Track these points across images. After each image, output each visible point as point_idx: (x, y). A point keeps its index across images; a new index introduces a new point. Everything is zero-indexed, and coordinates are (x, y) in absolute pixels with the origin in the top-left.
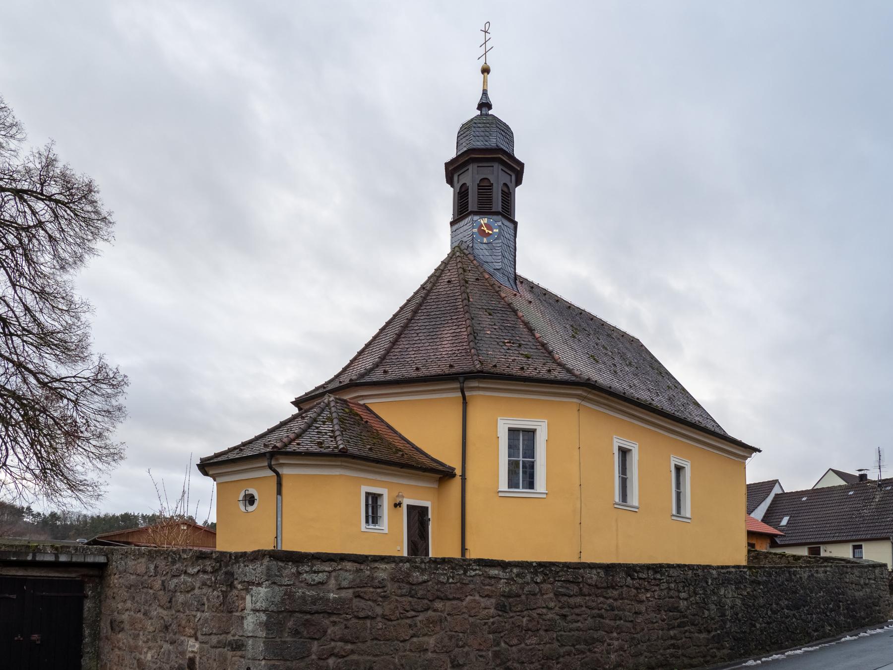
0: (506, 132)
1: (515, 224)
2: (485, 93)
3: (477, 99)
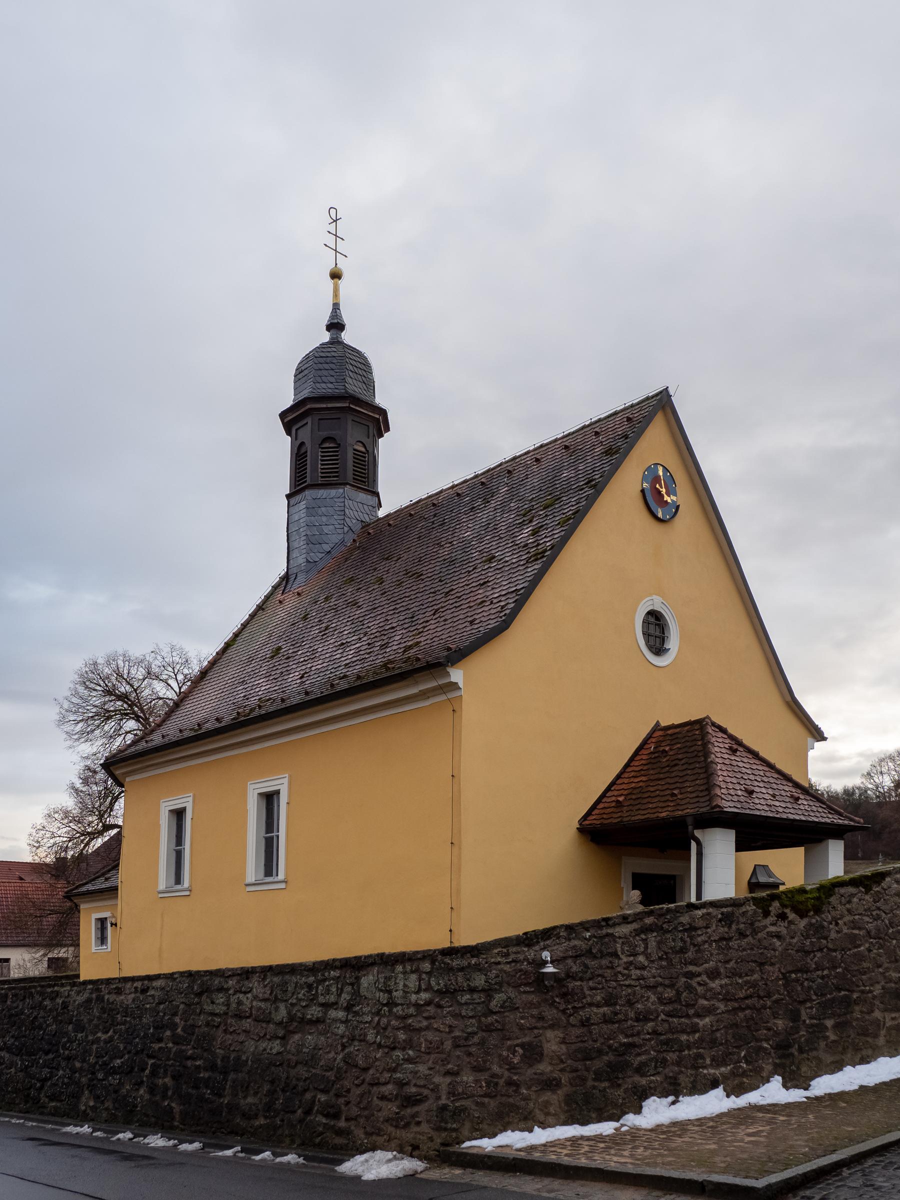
2: (336, 307)
3: (325, 319)
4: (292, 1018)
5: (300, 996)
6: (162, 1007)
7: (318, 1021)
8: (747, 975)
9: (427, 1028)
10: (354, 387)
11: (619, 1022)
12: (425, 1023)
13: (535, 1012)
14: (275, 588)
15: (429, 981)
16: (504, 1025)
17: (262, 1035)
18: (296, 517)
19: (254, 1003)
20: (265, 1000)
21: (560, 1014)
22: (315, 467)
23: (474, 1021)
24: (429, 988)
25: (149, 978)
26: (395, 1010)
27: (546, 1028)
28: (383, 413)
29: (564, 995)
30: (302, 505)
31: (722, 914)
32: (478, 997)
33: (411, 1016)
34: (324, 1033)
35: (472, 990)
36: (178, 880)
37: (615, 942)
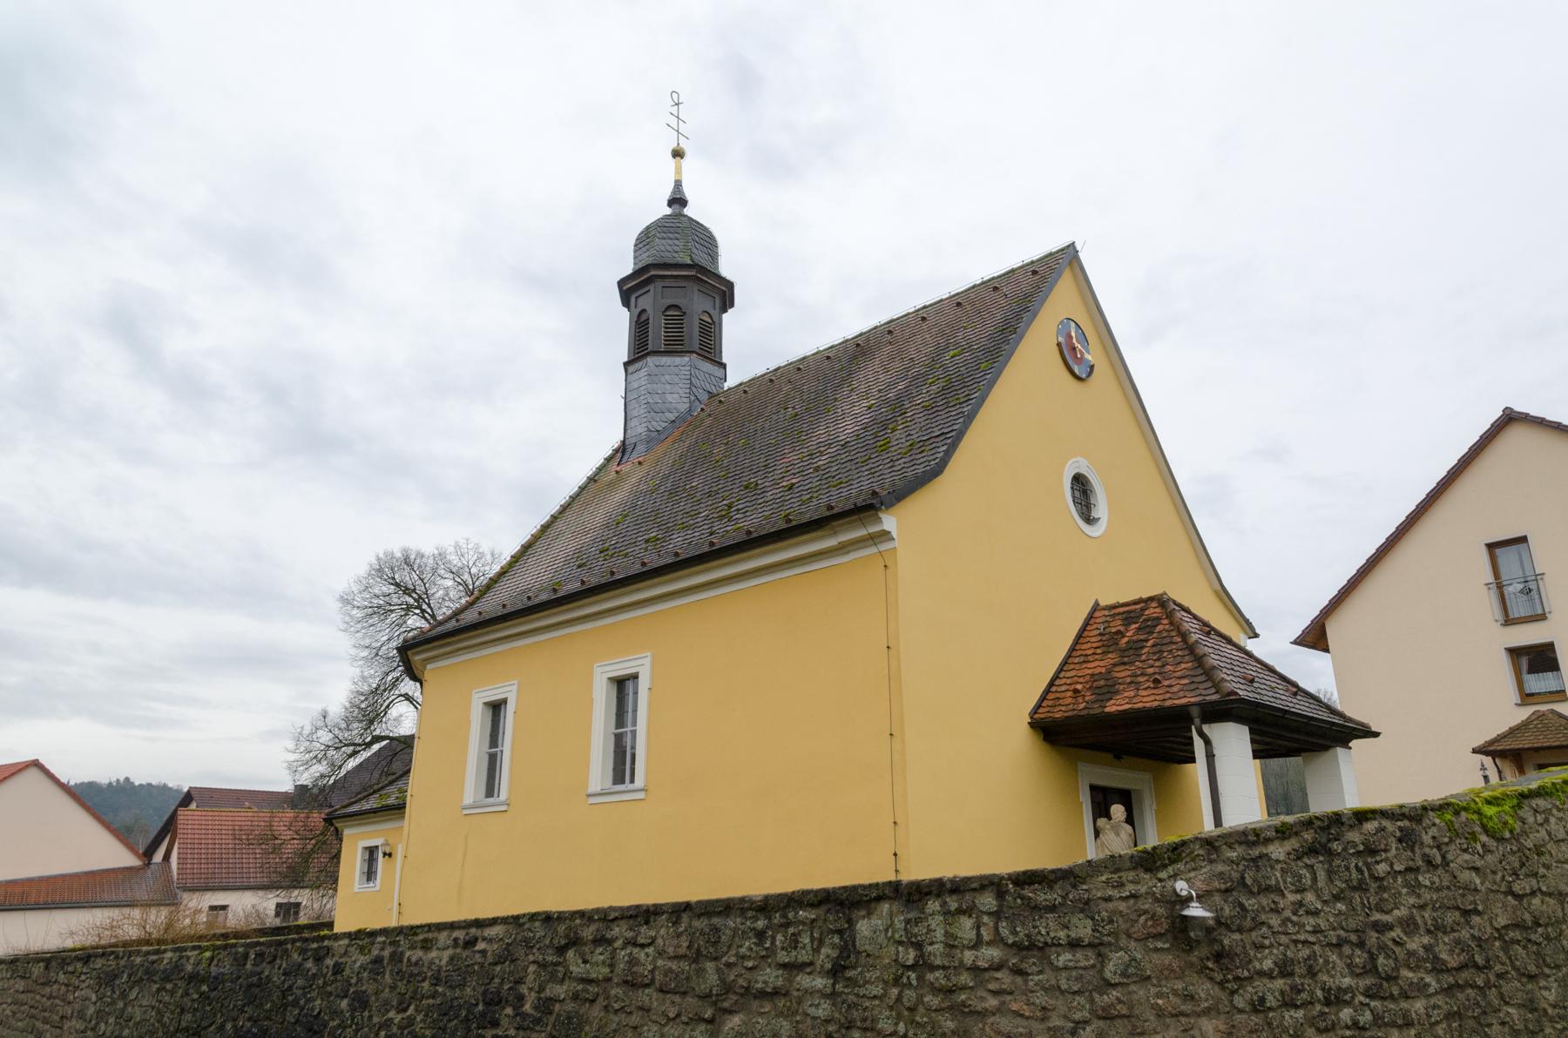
0: (707, 241)
1: (724, 366)
2: (678, 184)
3: (667, 192)
4: (728, 988)
5: (743, 950)
6: (498, 968)
7: (776, 993)
8: (1453, 930)
9: (998, 1011)
10: (702, 259)
11: (1305, 1004)
12: (993, 1002)
13: (1179, 985)
14: (609, 460)
15: (996, 929)
16: (1131, 1007)
17: (672, 1015)
18: (635, 385)
19: (660, 963)
20: (677, 957)
21: (1217, 989)
22: (658, 333)
23: (1082, 1000)
24: (997, 940)
25: (479, 924)
26: (930, 977)
27: (1199, 1015)
28: (730, 285)
29: (1218, 957)
30: (643, 373)
31: (1401, 829)
32: (1085, 958)
33: (964, 988)
34: (788, 1014)
35: (1074, 945)
36: (490, 790)
37: (1272, 868)
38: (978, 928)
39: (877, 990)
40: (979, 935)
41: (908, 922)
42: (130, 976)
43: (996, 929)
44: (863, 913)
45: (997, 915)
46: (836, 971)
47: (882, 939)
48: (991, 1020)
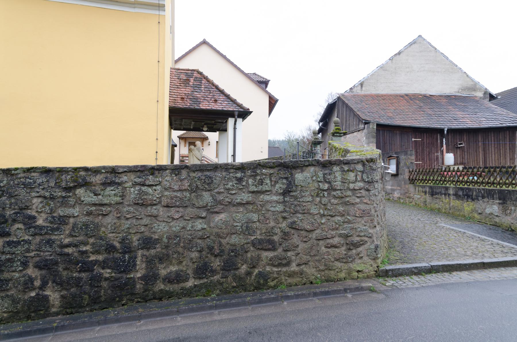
7: (248, 203)
12: (358, 200)
15: (362, 176)
24: (363, 180)
38: (356, 176)
39: (310, 199)
40: (356, 178)
41: (324, 174)
42: (458, 247)
43: (362, 176)
44: (299, 171)
45: (363, 172)
46: (286, 193)
47: (310, 180)
48: (357, 206)
